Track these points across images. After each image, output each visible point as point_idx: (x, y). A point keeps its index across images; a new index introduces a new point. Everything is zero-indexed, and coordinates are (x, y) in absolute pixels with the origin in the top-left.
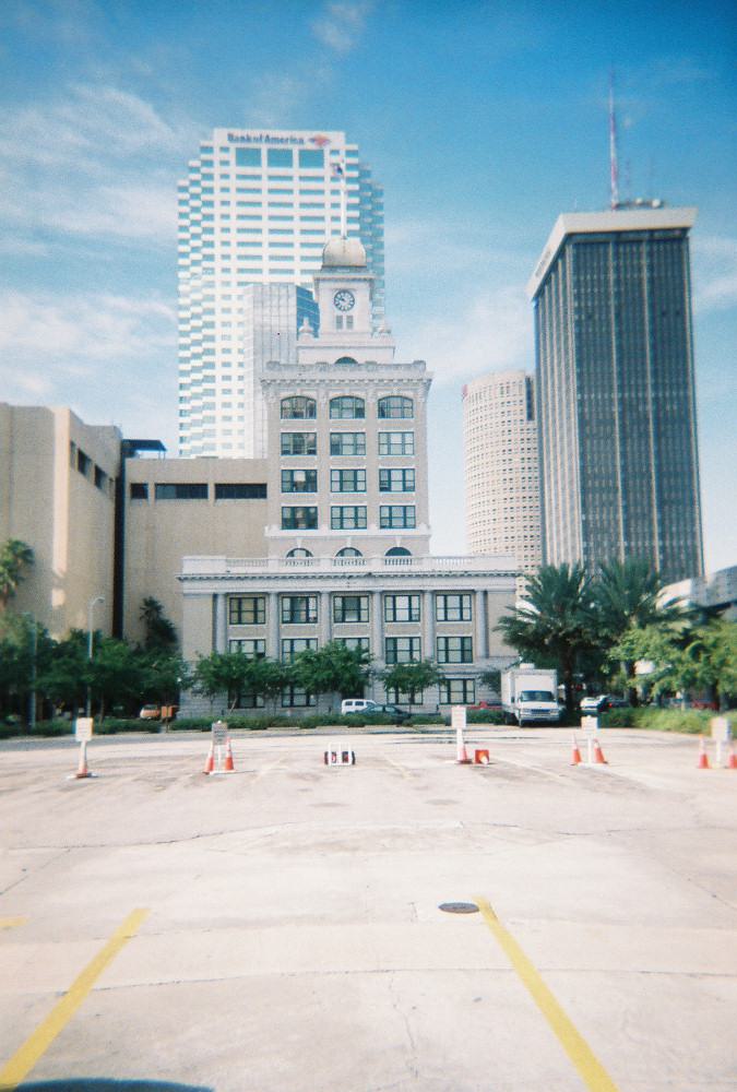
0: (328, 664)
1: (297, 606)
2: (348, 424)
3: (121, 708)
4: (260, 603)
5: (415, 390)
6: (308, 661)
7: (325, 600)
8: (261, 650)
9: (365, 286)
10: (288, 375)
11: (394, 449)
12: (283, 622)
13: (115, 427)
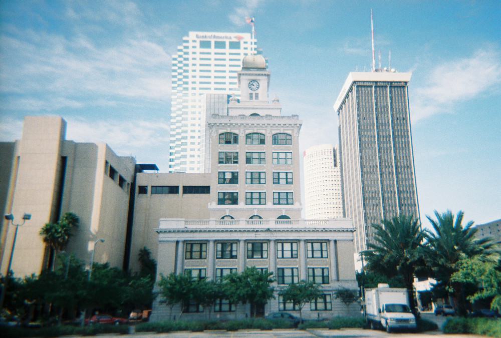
0: (246, 283)
1: (226, 248)
2: (256, 147)
3: (121, 311)
4: (204, 246)
5: (293, 131)
6: (233, 281)
7: (242, 244)
8: (203, 275)
9: (266, 77)
10: (223, 121)
11: (281, 161)
12: (217, 258)
13: (132, 157)
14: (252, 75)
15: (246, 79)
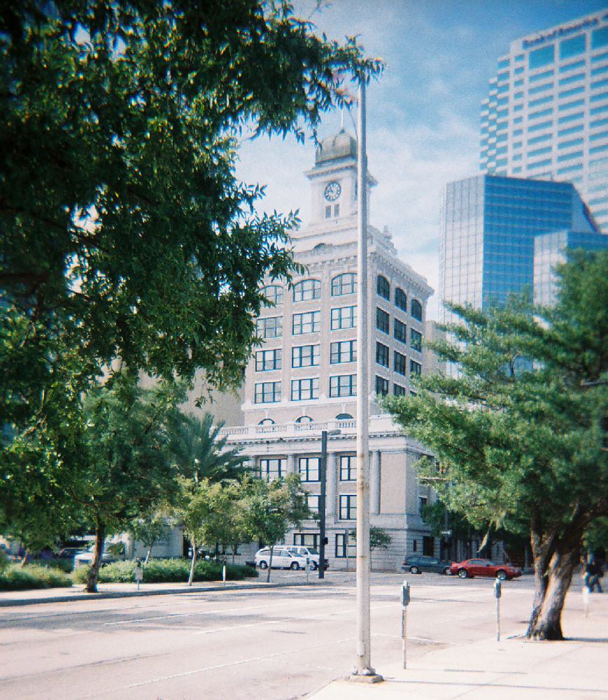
9: (348, 173)
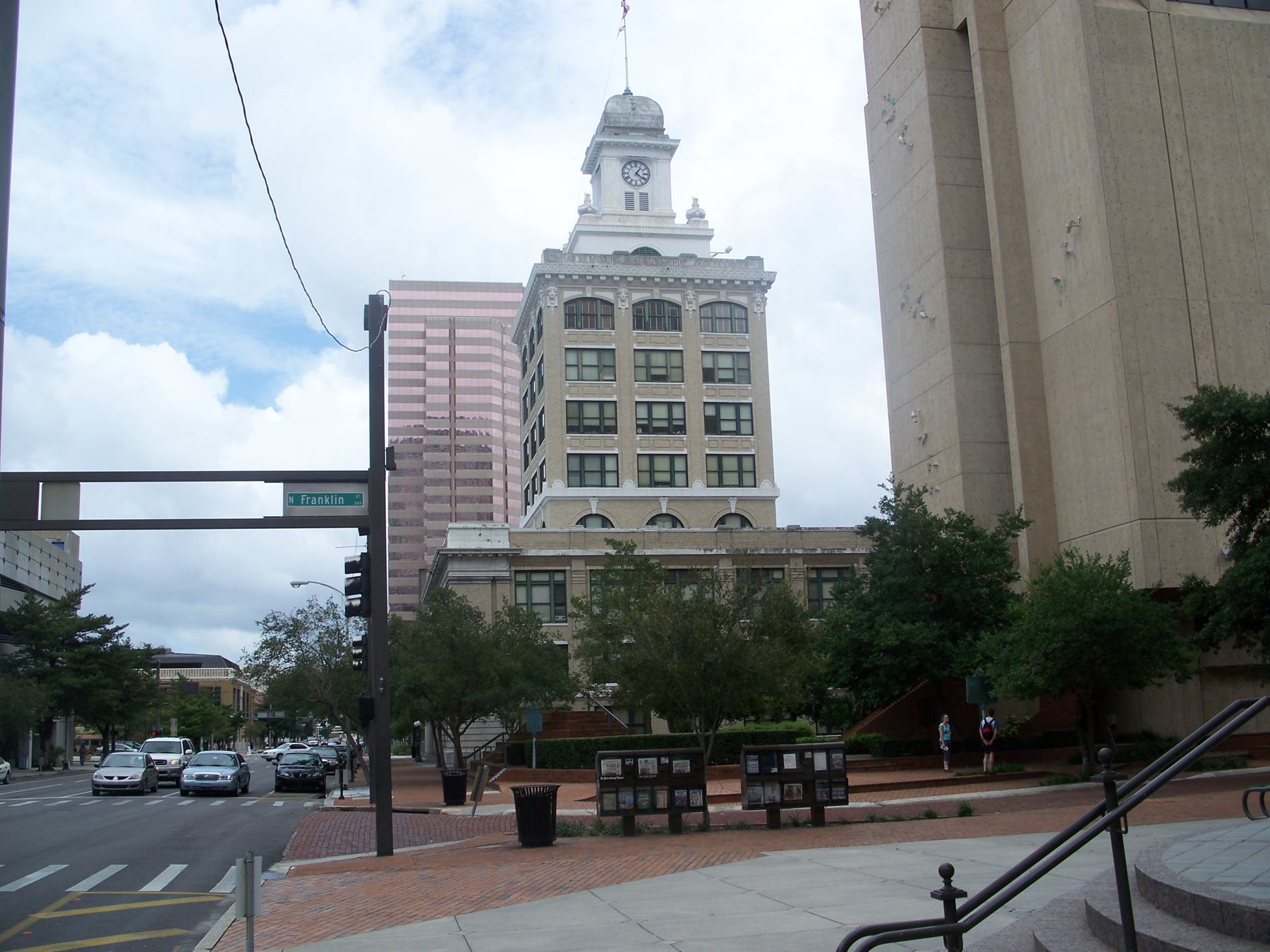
14: (632, 146)
15: (618, 157)
